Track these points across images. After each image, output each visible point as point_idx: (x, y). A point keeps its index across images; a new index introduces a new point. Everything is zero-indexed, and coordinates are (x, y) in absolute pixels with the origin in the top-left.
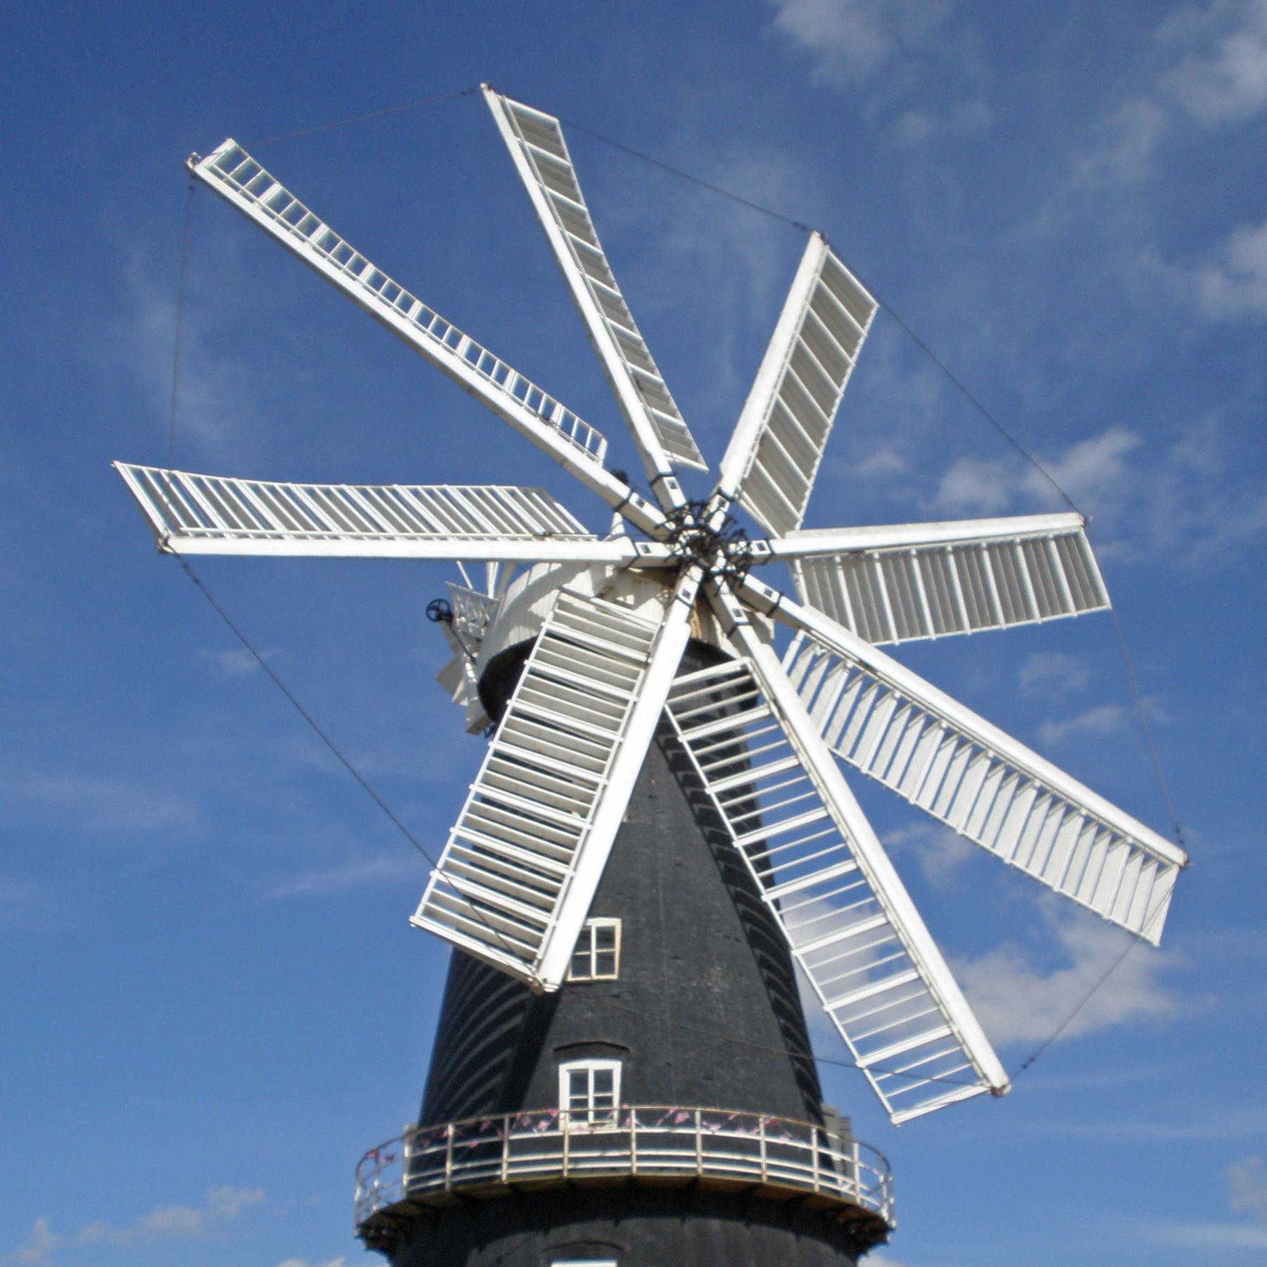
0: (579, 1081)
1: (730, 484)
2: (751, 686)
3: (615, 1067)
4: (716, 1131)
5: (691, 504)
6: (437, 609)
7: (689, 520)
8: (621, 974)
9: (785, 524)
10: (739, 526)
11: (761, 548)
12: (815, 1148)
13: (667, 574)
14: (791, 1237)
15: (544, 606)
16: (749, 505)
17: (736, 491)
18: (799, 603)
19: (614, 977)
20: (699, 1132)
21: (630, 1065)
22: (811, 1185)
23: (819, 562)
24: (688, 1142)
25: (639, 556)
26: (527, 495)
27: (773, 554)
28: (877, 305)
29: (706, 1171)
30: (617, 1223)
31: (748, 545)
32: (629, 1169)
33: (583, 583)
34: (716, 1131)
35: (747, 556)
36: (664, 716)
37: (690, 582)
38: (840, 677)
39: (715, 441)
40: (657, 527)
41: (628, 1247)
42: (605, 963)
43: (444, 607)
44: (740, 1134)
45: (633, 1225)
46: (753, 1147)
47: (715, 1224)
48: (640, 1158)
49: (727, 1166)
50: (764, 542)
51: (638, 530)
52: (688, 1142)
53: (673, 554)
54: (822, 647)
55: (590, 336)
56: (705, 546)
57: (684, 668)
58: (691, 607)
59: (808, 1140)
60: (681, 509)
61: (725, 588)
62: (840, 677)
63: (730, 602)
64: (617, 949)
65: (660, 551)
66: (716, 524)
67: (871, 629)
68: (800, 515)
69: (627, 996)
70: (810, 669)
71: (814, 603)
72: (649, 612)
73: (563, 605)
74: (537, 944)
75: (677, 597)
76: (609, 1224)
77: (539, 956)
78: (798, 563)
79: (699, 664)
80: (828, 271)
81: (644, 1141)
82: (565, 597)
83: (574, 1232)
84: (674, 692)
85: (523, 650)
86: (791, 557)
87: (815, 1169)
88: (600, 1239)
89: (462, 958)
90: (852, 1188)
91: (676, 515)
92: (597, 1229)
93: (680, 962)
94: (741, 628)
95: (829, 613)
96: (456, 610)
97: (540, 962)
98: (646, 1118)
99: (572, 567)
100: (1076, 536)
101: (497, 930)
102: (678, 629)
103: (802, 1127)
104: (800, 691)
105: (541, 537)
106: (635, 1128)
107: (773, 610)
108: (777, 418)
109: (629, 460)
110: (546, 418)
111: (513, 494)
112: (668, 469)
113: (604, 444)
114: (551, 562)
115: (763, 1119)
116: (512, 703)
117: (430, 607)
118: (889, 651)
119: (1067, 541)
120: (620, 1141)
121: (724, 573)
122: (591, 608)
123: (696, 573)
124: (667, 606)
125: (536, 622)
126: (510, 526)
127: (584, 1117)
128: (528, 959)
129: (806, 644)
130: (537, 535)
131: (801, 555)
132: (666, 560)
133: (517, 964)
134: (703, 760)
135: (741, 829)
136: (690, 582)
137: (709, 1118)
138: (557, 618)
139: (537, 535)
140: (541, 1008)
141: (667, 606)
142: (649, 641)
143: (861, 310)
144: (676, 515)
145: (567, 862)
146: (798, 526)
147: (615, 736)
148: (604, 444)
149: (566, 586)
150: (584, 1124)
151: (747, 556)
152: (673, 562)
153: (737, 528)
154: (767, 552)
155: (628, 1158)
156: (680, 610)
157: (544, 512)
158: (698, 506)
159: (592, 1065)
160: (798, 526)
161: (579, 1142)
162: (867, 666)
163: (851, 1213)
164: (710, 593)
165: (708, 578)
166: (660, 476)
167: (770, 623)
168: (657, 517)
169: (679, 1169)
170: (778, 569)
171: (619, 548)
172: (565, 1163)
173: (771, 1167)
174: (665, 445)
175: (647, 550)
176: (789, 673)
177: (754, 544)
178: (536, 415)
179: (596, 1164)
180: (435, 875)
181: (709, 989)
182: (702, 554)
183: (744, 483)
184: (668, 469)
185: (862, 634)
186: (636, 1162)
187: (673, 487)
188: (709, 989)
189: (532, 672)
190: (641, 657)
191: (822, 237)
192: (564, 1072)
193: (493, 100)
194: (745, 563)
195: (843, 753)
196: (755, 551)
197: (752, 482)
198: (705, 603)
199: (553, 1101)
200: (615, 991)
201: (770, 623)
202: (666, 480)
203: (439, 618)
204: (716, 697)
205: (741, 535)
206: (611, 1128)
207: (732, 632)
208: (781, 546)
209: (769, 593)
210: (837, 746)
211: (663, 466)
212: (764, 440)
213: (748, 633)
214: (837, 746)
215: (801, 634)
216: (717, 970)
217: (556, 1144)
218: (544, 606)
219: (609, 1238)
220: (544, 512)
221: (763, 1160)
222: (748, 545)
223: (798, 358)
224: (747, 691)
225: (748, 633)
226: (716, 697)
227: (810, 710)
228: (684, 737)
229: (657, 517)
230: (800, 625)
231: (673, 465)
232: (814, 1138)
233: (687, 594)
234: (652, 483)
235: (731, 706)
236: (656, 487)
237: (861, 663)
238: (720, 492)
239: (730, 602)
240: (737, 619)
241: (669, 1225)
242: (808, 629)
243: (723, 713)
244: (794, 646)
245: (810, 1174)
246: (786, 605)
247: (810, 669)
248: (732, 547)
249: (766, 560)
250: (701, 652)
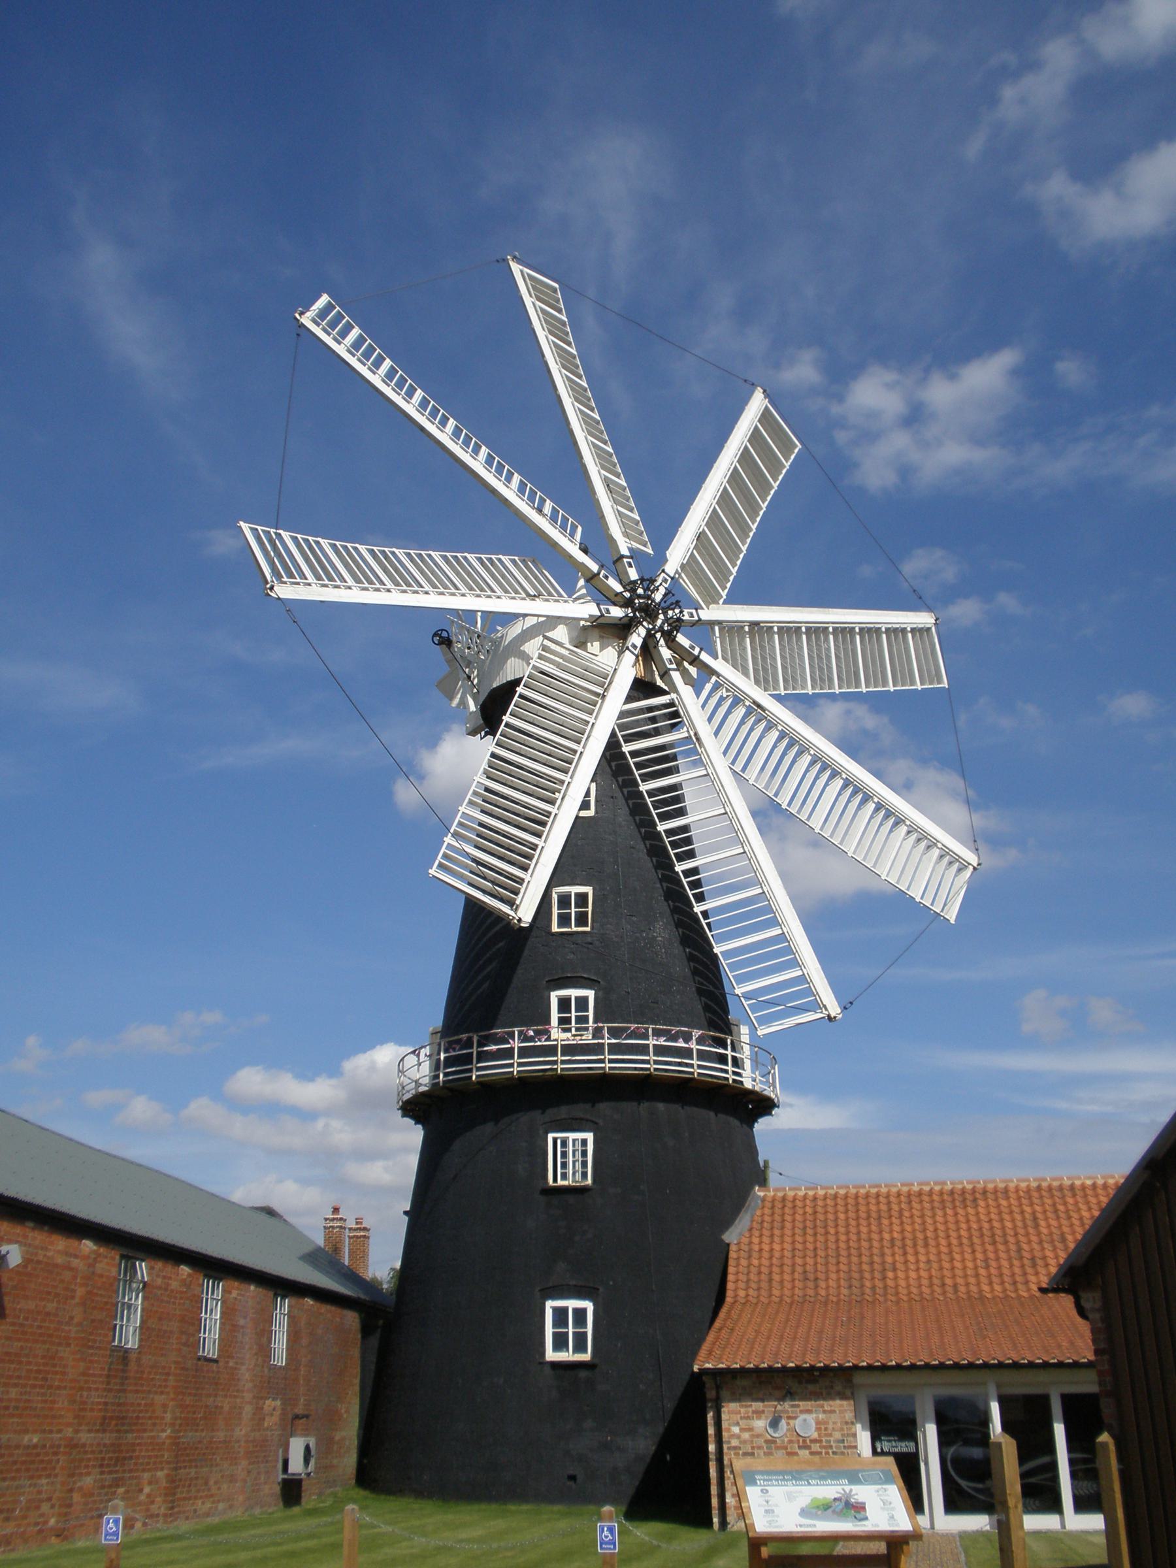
0: (564, 1004)
1: (671, 567)
2: (676, 714)
3: (590, 994)
4: (662, 1041)
5: (642, 580)
6: (440, 637)
7: (640, 591)
8: (592, 928)
9: (712, 598)
10: (675, 598)
11: (691, 615)
12: (729, 1052)
13: (622, 630)
14: (712, 1114)
15: (532, 647)
16: (686, 583)
17: (677, 572)
18: (716, 657)
19: (588, 929)
20: (652, 1042)
21: (600, 994)
22: (727, 1079)
23: (732, 629)
24: (644, 1050)
25: (602, 615)
26: (524, 562)
27: (700, 620)
28: (800, 446)
29: (656, 1069)
30: (593, 1106)
31: (681, 612)
32: (604, 1068)
33: (561, 633)
34: (662, 1041)
35: (679, 620)
36: (613, 734)
37: (637, 638)
38: (740, 711)
39: (663, 535)
40: (617, 594)
41: (601, 1122)
42: (582, 919)
43: (445, 634)
44: (681, 1044)
45: (604, 1107)
46: (687, 1053)
47: (661, 1106)
48: (611, 1061)
49: (670, 1066)
50: (694, 611)
51: (603, 596)
52: (644, 1050)
53: (627, 615)
54: (728, 690)
55: (575, 443)
56: (649, 612)
57: (629, 699)
58: (637, 657)
59: (726, 1049)
60: (635, 582)
61: (662, 642)
62: (740, 711)
63: (666, 653)
64: (590, 909)
65: (617, 612)
66: (658, 596)
67: (764, 680)
68: (724, 594)
69: (597, 943)
70: (718, 705)
71: (724, 658)
72: (603, 655)
73: (545, 648)
74: (516, 893)
75: (628, 648)
76: (588, 1106)
77: (518, 902)
78: (717, 628)
79: (641, 696)
80: (765, 417)
81: (614, 1049)
82: (546, 642)
83: (563, 1112)
84: (623, 714)
85: (517, 682)
86: (712, 624)
87: (730, 1068)
88: (582, 1116)
89: (472, 905)
90: (749, 1079)
91: (631, 586)
92: (579, 1110)
93: (634, 919)
94: (672, 673)
95: (735, 666)
96: (454, 639)
97: (518, 907)
98: (614, 1033)
99: (553, 621)
100: (929, 629)
101: (493, 883)
102: (627, 671)
103: (720, 1038)
104: (710, 720)
105: (533, 597)
106: (607, 1041)
107: (695, 661)
108: (713, 520)
109: (596, 540)
110: (540, 510)
111: (514, 562)
112: (627, 553)
113: (580, 529)
114: (538, 616)
115: (696, 1033)
116: (506, 718)
117: (435, 635)
118: (778, 698)
119: (920, 632)
120: (597, 1049)
121: (661, 629)
122: (566, 653)
123: (642, 631)
124: (620, 653)
125: (526, 658)
126: (511, 588)
127: (569, 1030)
128: (511, 903)
129: (717, 686)
130: (528, 595)
131: (719, 623)
132: (621, 619)
133: (505, 909)
134: (639, 766)
135: (664, 817)
136: (637, 638)
137: (658, 1034)
138: (541, 657)
139: (528, 595)
140: (516, 937)
141: (620, 653)
142: (605, 680)
143: (787, 447)
144: (631, 586)
145: (540, 836)
146: (721, 601)
147: (579, 749)
148: (580, 529)
149: (549, 634)
150: (568, 1035)
151: (679, 620)
152: (625, 621)
153: (673, 600)
154: (696, 618)
155: (602, 1061)
156: (629, 658)
157: (536, 578)
158: (648, 582)
159: (574, 993)
160: (721, 601)
161: (569, 1050)
162: (759, 706)
163: (752, 1097)
164: (651, 644)
165: (650, 636)
166: (623, 557)
167: (693, 671)
168: (618, 588)
169: (635, 1069)
170: (701, 629)
171: (586, 610)
172: (561, 1064)
173: (700, 1067)
174: (626, 534)
175: (608, 611)
176: (703, 706)
177: (686, 612)
178: (533, 508)
179: (583, 1064)
180: (448, 839)
181: (654, 938)
182: (642, 615)
183: (683, 566)
184: (627, 553)
185: (757, 682)
186: (608, 1064)
187: (630, 566)
188: (654, 938)
189: (521, 696)
190: (600, 691)
191: (765, 391)
192: (554, 996)
193: (516, 268)
194: (677, 624)
195: (738, 770)
196: (686, 617)
197: (689, 566)
198: (647, 652)
199: (547, 1021)
200: (589, 939)
201: (693, 671)
202: (625, 560)
203: (440, 643)
204: (653, 720)
205: (677, 604)
206: (588, 1038)
207: (665, 674)
208: (706, 614)
209: (693, 648)
210: (733, 763)
211: (625, 551)
212: (701, 537)
213: (676, 676)
214: (733, 763)
215: (714, 679)
216: (659, 925)
217: (551, 1051)
218: (532, 647)
219: (588, 1117)
220: (536, 578)
221: (695, 1062)
222: (681, 612)
223: (734, 478)
224: (674, 717)
225: (676, 676)
226: (653, 720)
227: (716, 734)
228: (626, 748)
229: (618, 588)
230: (713, 672)
231: (630, 549)
232: (729, 1048)
233: (635, 647)
234: (615, 562)
235: (642, 719)
236: (618, 565)
237: (754, 702)
238: (663, 571)
239: (666, 653)
240: (669, 666)
241: (628, 1107)
242: (718, 675)
243: (657, 732)
244: (708, 687)
245: (726, 1071)
246: (705, 657)
247: (718, 705)
248: (670, 613)
249: (694, 624)
250: (642, 688)
